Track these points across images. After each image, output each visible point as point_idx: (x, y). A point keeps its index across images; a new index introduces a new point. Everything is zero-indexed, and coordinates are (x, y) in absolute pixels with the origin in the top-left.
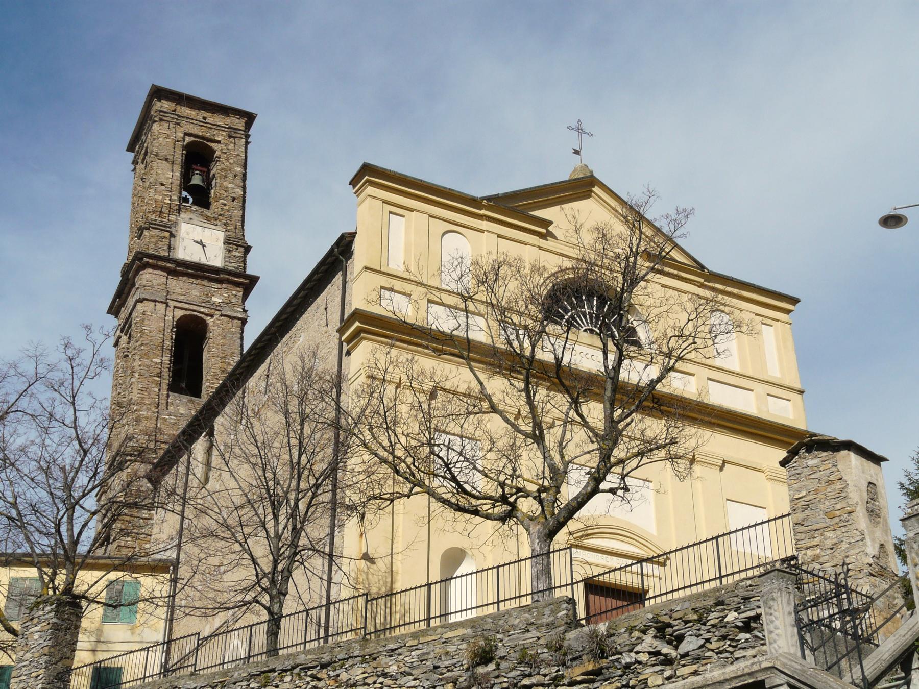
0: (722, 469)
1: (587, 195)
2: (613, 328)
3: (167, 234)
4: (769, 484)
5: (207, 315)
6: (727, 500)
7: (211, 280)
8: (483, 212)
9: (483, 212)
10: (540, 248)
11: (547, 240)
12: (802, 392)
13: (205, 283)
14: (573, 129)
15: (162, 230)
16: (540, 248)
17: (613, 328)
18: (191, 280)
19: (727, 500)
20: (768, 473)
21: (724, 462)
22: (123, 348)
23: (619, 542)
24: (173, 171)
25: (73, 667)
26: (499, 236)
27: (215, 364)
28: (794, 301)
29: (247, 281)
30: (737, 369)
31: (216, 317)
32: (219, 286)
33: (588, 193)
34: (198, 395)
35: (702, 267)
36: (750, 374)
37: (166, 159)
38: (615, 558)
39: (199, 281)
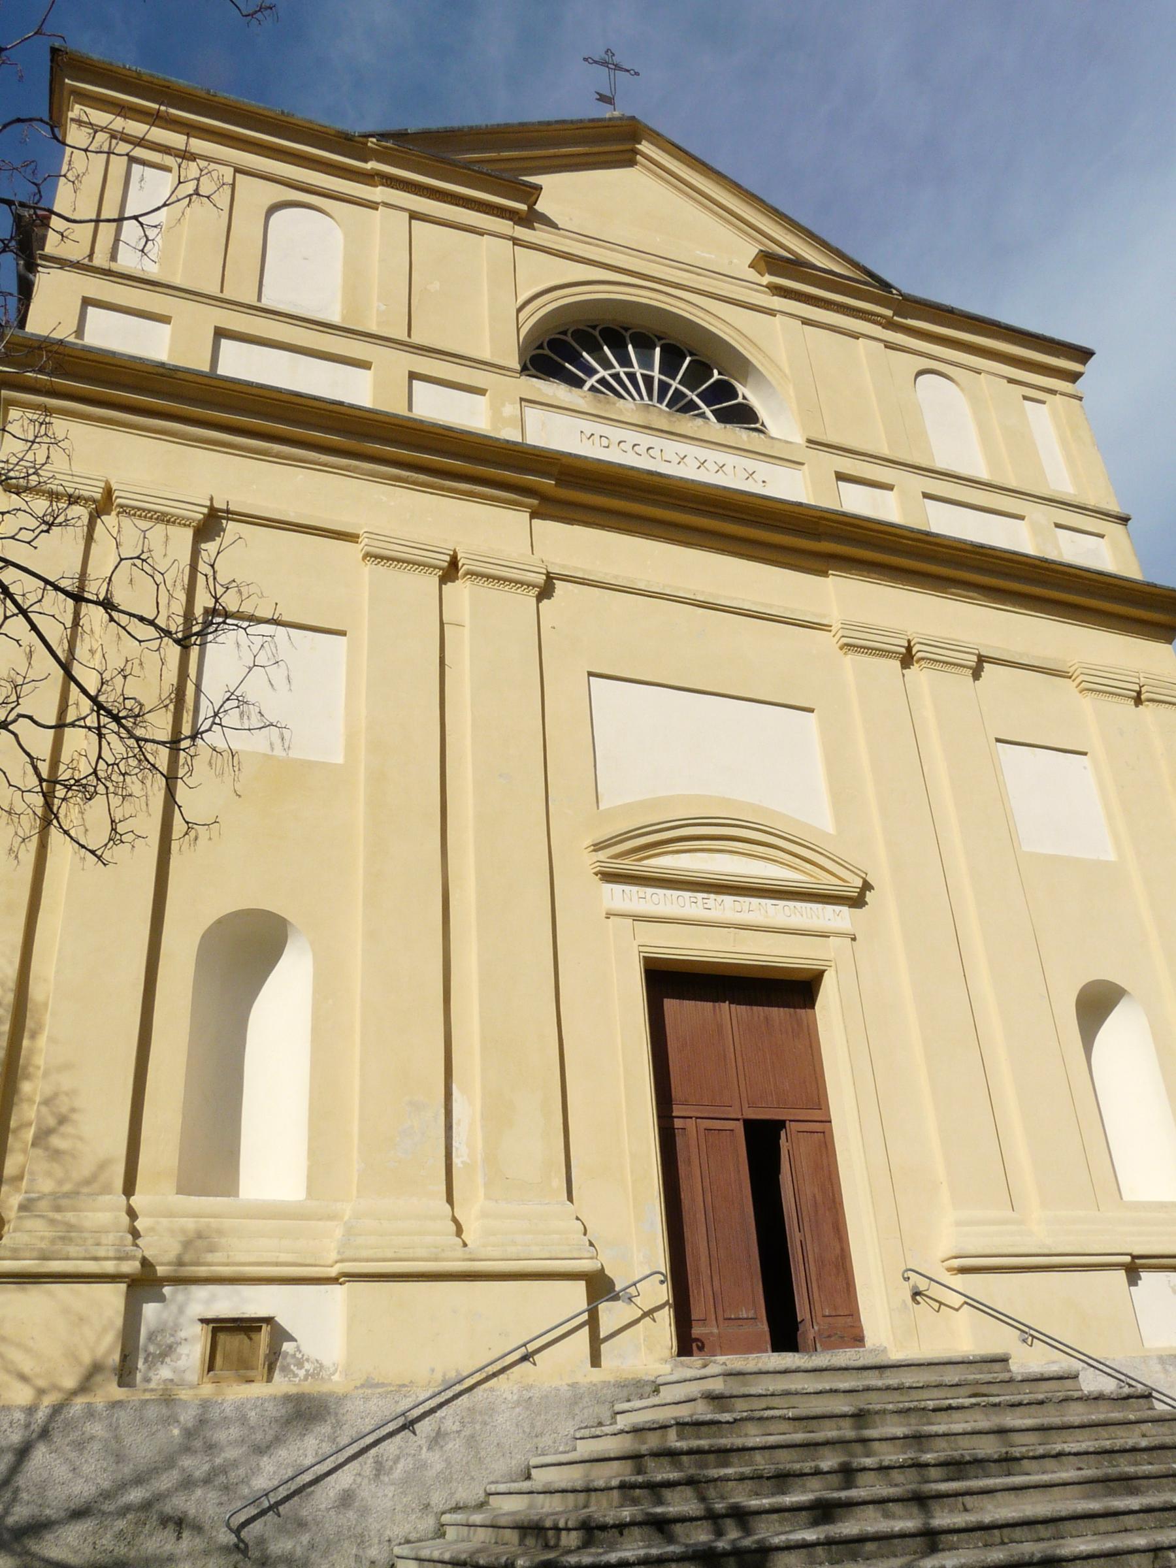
0: (977, 674)
1: (628, 159)
4: (1087, 703)
6: (998, 740)
8: (371, 165)
9: (371, 165)
10: (516, 241)
11: (534, 229)
12: (1124, 520)
14: (595, 62)
16: (516, 241)
19: (998, 740)
20: (1082, 678)
21: (982, 660)
23: (736, 857)
25: (587, 1328)
26: (414, 216)
28: (1084, 355)
30: (984, 475)
33: (627, 156)
35: (886, 286)
36: (1013, 484)
38: (728, 900)
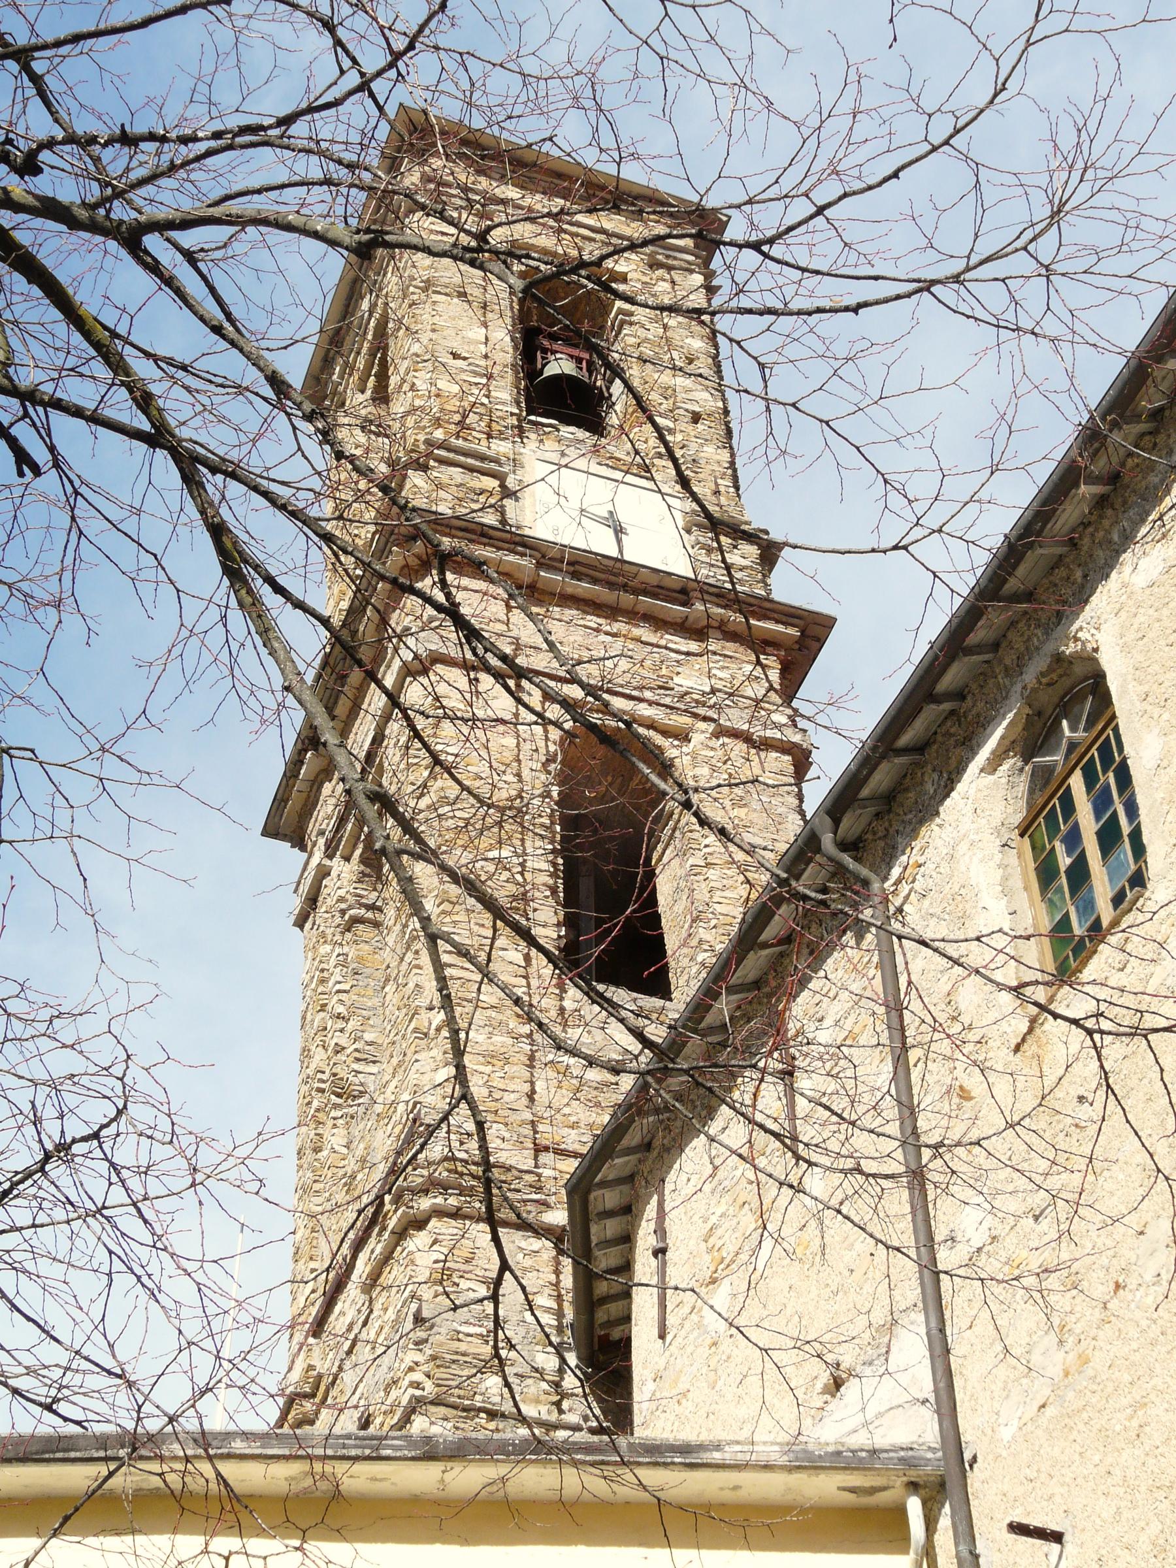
2: (641, 765)
3: (491, 483)
5: (666, 733)
7: (659, 623)
13: (644, 632)
15: (471, 469)
17: (641, 765)
18: (593, 621)
22: (341, 900)
24: (485, 325)
27: (724, 888)
29: (793, 632)
31: (697, 738)
32: (693, 646)
34: (659, 986)
37: (463, 295)
39: (618, 626)
